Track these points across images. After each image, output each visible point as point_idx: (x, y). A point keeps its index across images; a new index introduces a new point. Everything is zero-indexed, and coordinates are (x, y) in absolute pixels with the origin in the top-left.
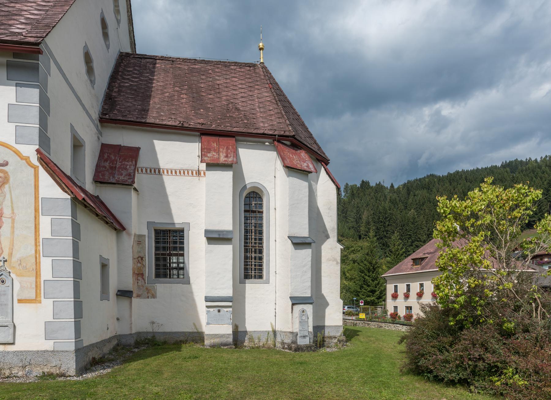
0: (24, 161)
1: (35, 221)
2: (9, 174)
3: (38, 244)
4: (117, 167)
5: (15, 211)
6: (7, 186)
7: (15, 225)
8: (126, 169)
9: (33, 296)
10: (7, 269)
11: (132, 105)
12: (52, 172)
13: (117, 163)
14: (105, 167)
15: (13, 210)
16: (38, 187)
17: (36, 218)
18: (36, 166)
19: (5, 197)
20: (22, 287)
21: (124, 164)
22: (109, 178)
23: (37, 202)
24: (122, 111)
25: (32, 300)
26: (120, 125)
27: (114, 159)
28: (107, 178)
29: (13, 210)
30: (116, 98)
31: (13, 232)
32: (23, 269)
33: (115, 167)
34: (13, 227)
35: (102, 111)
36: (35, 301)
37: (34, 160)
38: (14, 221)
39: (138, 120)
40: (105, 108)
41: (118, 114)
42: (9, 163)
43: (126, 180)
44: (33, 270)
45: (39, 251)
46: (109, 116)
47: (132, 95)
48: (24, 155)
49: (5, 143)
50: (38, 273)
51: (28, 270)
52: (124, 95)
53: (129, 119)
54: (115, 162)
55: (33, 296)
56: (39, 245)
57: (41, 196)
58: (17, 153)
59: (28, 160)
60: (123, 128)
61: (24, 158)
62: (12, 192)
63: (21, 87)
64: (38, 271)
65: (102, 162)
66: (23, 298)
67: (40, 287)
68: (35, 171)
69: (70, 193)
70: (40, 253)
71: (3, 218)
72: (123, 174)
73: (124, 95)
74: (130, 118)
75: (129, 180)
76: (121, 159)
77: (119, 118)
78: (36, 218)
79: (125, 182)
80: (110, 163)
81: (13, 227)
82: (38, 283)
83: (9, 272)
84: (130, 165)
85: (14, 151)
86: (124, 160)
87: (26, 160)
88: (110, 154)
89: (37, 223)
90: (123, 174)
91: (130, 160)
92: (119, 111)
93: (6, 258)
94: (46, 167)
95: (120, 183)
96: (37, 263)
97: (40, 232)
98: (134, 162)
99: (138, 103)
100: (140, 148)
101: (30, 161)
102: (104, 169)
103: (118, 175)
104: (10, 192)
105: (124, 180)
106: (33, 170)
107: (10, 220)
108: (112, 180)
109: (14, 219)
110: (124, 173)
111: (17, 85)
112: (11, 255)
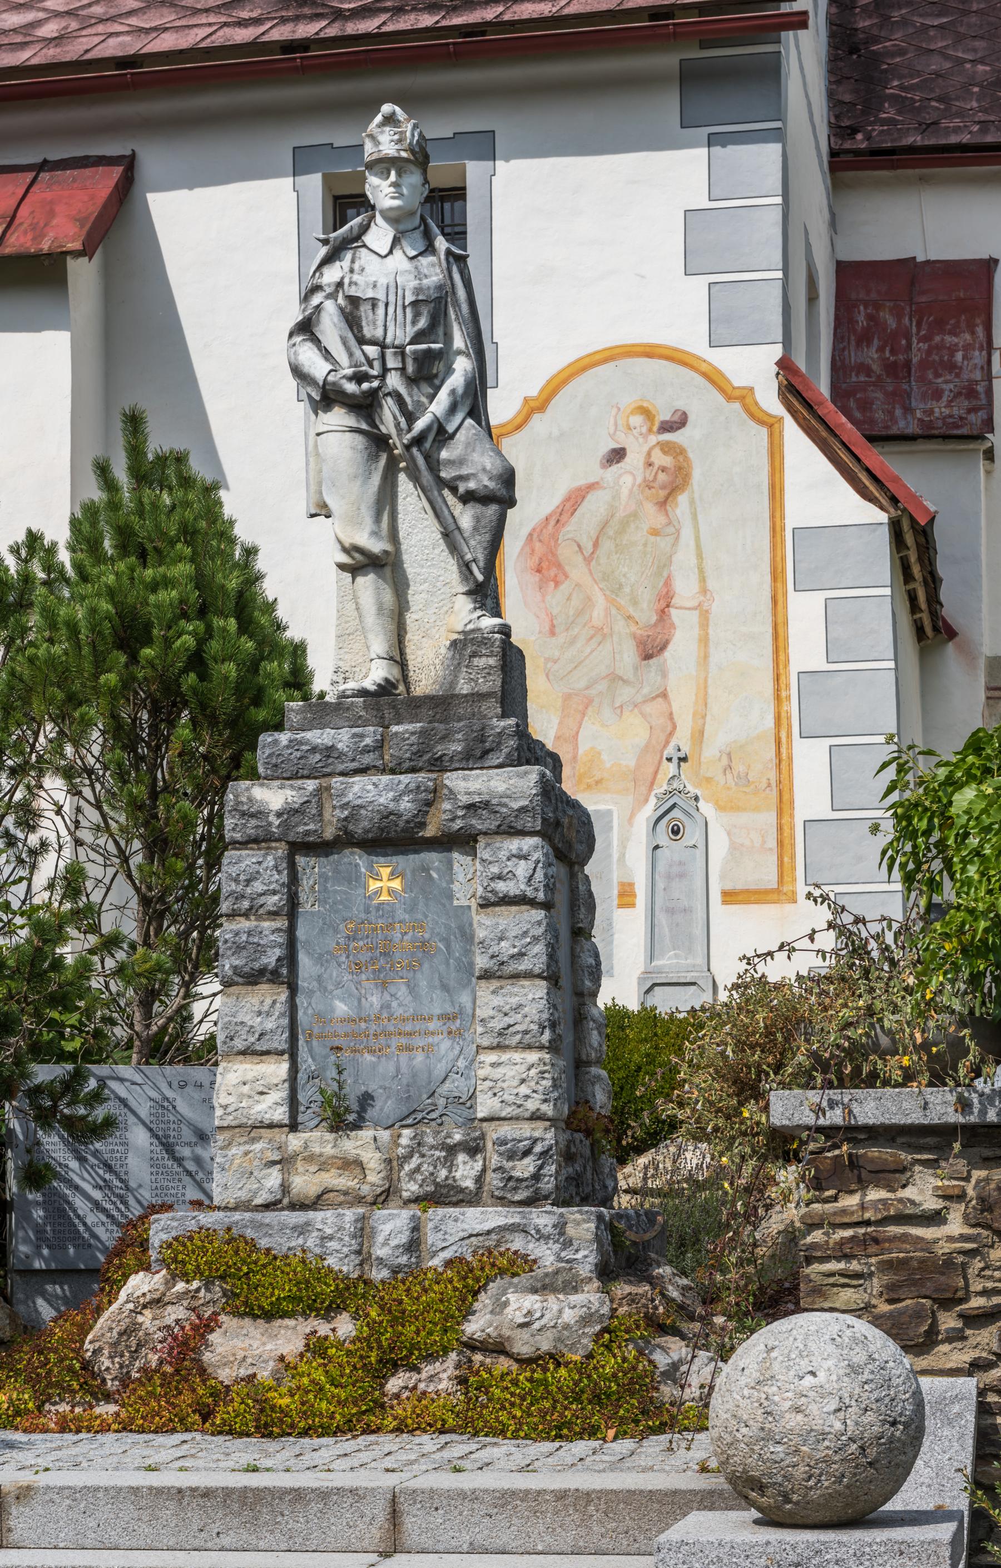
0: (737, 406)
1: (775, 614)
2: (691, 455)
3: (784, 694)
4: (915, 360)
5: (711, 584)
6: (683, 499)
7: (711, 631)
8: (952, 367)
9: (769, 878)
10: (689, 788)
11: (948, 65)
12: (824, 434)
13: (909, 346)
14: (868, 370)
15: (703, 580)
16: (782, 490)
17: (778, 601)
18: (775, 417)
19: (677, 538)
20: (735, 848)
21: (940, 347)
22: (891, 413)
23: (779, 546)
24: (915, 101)
25: (767, 892)
26: (910, 172)
27: (894, 326)
28: (879, 415)
29: (703, 580)
30: (876, 40)
31: (706, 657)
32: (736, 784)
33: (908, 364)
34: (704, 641)
35: (833, 120)
36: (775, 897)
37: (771, 401)
38: (707, 619)
39: (989, 139)
40: (841, 103)
41: (902, 123)
42: (691, 418)
43: (961, 418)
44: (769, 785)
45: (789, 718)
46: (868, 138)
47: (940, 15)
48: (736, 384)
49: (676, 350)
50: (786, 797)
51: (752, 787)
52: (904, 22)
53: (954, 139)
54: (904, 342)
55: (769, 878)
56: (789, 698)
57: (790, 524)
58: (715, 378)
59: (749, 400)
60: (923, 180)
61: (737, 393)
62: (700, 517)
63: (724, 146)
64: (786, 789)
65: (852, 348)
66: (739, 886)
67: (793, 846)
68: (771, 435)
69: (884, 502)
70: (790, 727)
71: (673, 611)
72: (942, 391)
73: (904, 22)
74: (957, 130)
75: (972, 417)
76: (924, 326)
77: (909, 140)
78: (778, 601)
79: (958, 427)
80: (881, 349)
81: (704, 641)
82: (787, 832)
83: (696, 799)
84: (968, 348)
85: (705, 375)
86: (939, 325)
87: (742, 399)
88: (877, 307)
89: (780, 620)
90: (942, 391)
91: (963, 325)
92: (901, 103)
93: (686, 749)
94: (805, 418)
95: (936, 432)
96: (783, 761)
97: (791, 650)
98: (980, 331)
99: (975, 50)
100: (996, 261)
101: (756, 404)
102: (862, 378)
103: (924, 397)
104: (695, 516)
105: (951, 416)
106: (764, 431)
107: (694, 617)
108: (902, 424)
109: (707, 611)
110: (947, 385)
111: (712, 141)
112: (699, 736)
